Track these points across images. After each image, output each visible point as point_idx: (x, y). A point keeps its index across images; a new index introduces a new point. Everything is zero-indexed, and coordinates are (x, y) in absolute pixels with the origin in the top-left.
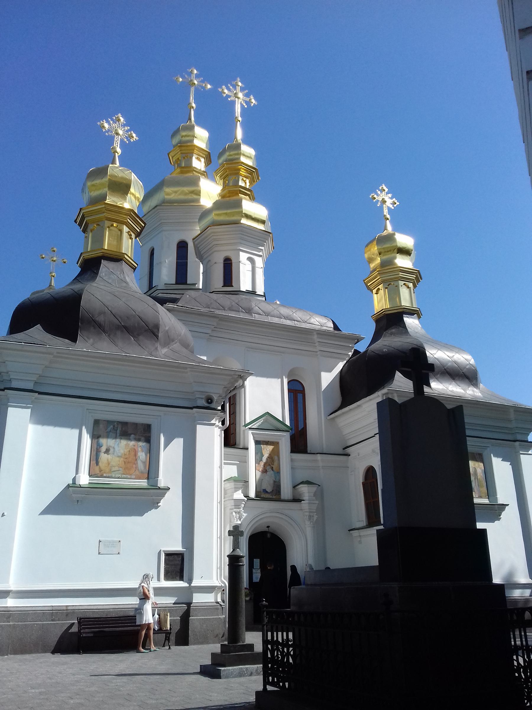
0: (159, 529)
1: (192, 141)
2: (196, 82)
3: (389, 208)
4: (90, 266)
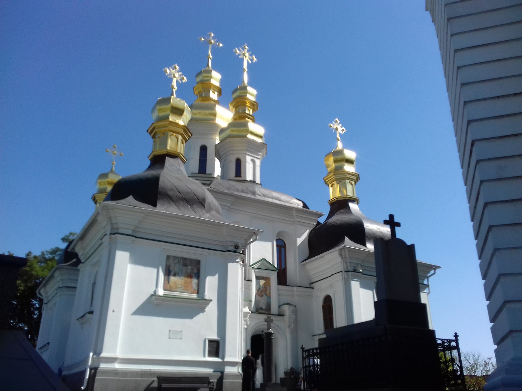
0: (205, 325)
1: (210, 80)
2: (213, 41)
3: (340, 134)
4: (158, 161)
